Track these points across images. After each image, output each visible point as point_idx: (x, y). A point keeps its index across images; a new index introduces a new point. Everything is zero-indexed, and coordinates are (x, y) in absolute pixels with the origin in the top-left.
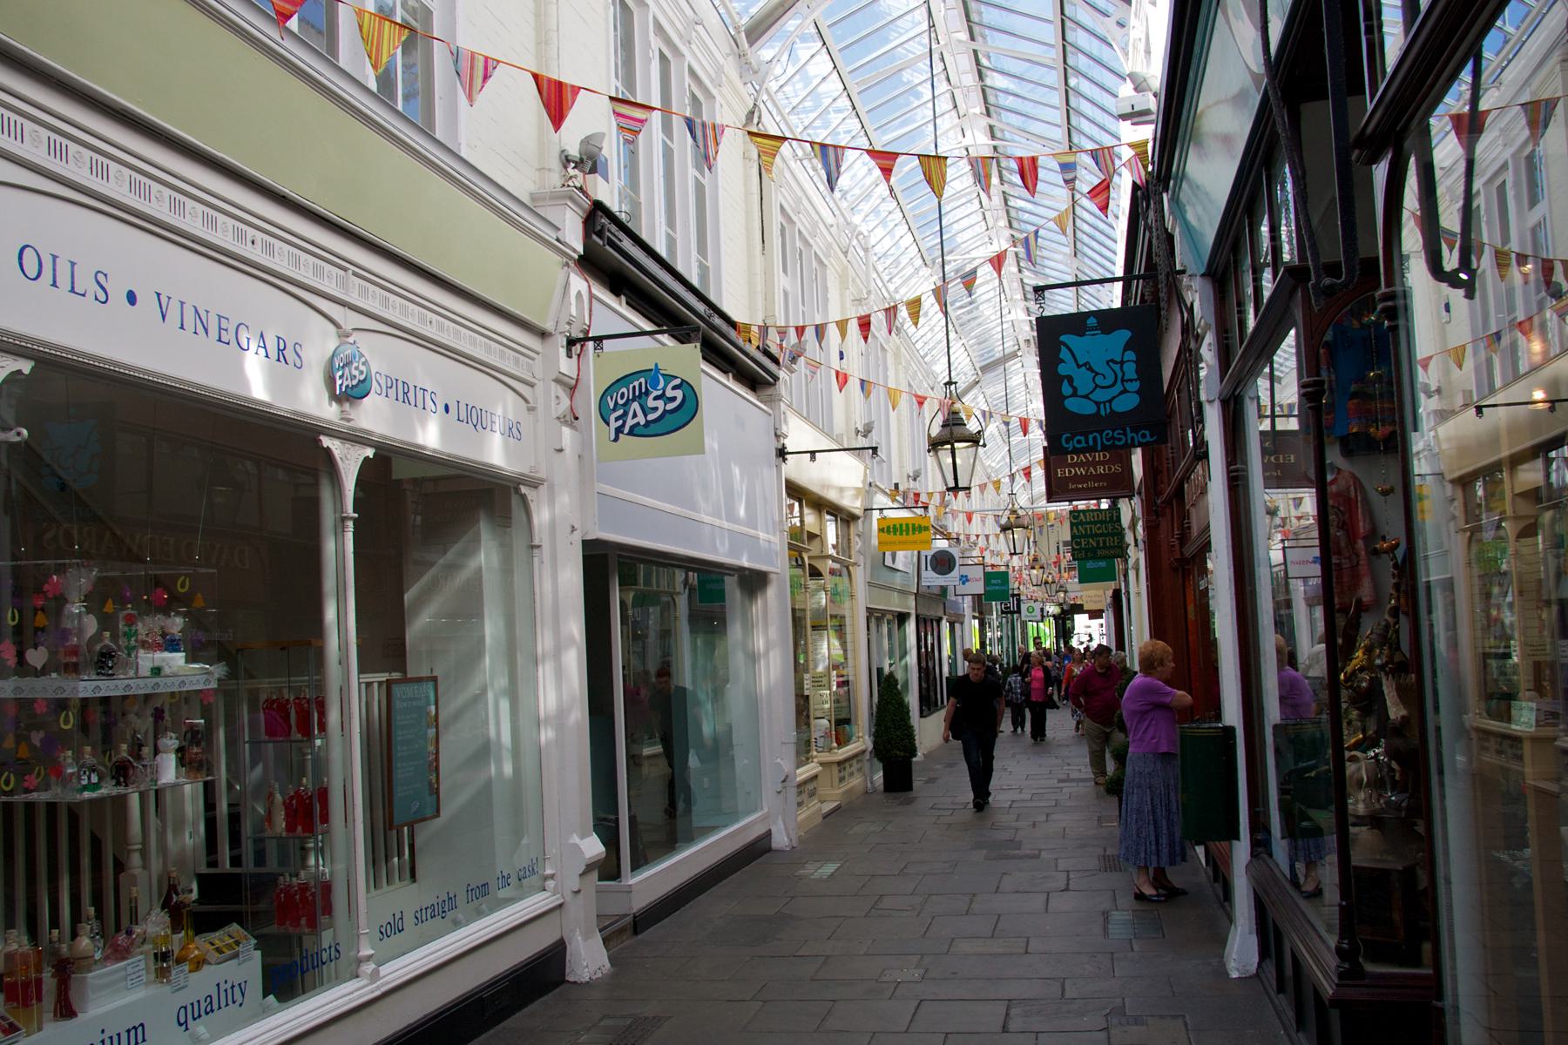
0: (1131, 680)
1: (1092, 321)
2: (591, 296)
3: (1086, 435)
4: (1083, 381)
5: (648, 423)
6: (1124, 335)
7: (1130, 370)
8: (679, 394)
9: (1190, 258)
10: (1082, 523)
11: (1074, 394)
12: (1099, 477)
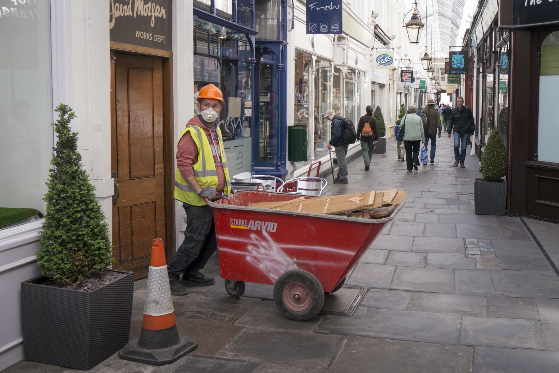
0: (186, 203)
1: (458, 53)
2: (375, 40)
3: (455, 71)
4: (456, 62)
5: (384, 63)
6: (462, 56)
7: (463, 61)
8: (390, 59)
9: (474, 45)
11: (454, 64)
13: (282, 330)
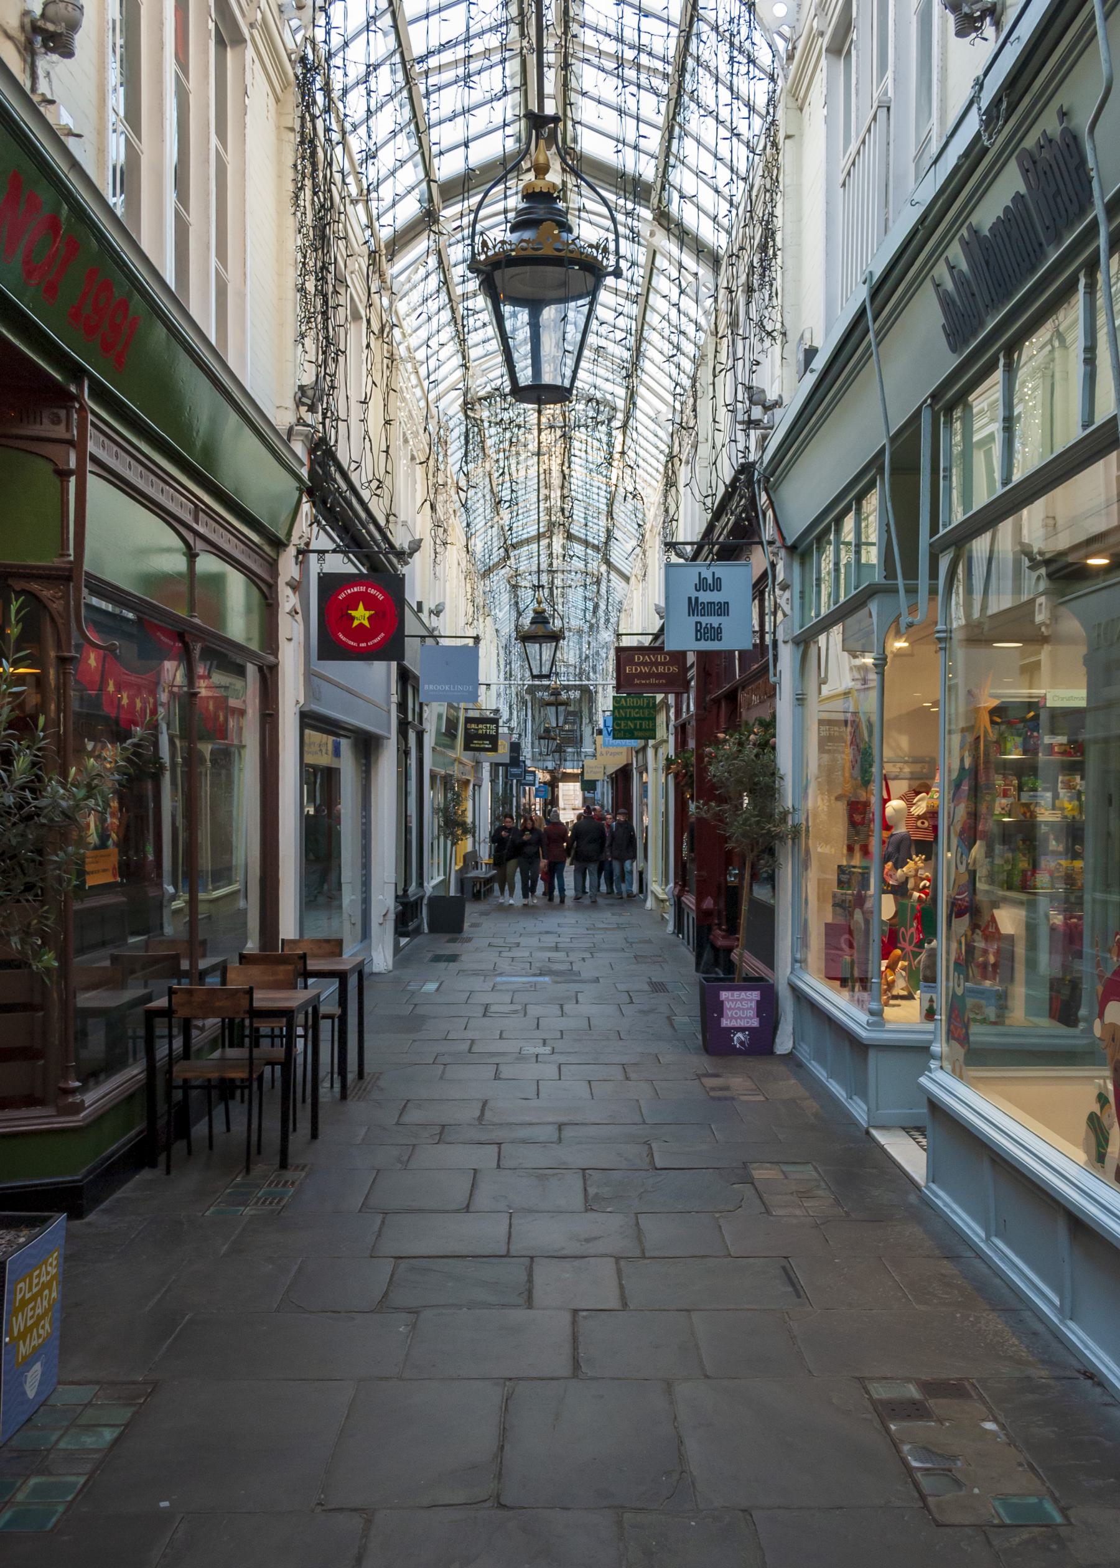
10: (622, 707)
12: (659, 676)
13: (168, 1342)
